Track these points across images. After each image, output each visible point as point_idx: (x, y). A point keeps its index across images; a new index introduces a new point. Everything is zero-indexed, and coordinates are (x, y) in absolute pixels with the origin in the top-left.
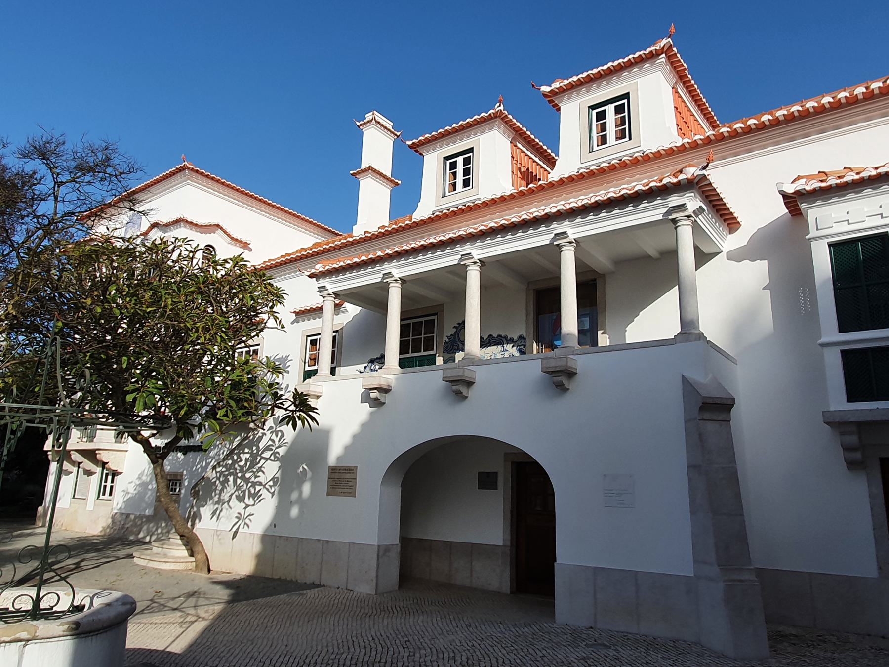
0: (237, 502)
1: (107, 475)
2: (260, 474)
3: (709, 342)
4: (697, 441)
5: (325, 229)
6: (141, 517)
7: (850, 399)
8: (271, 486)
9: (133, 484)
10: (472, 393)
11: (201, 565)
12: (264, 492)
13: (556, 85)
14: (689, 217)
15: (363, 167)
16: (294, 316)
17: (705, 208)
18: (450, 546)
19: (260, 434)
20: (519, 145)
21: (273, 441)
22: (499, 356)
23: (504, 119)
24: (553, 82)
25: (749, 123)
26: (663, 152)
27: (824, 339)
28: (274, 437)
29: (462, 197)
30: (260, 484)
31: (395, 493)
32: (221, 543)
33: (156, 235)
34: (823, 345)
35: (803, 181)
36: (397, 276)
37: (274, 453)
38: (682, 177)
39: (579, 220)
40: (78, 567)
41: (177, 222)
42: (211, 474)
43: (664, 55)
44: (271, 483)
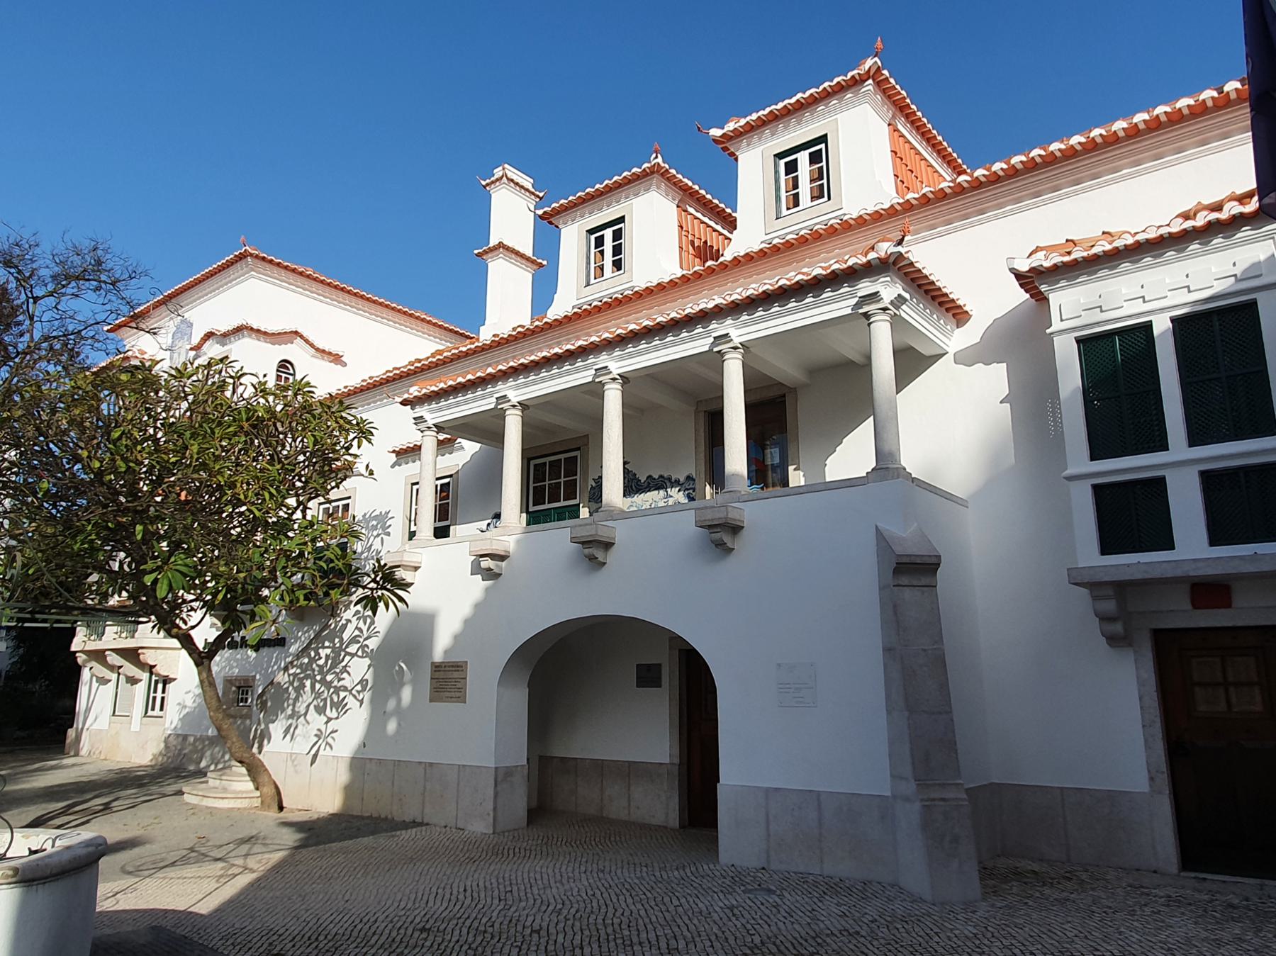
0: (316, 715)
1: (157, 682)
2: (345, 675)
3: (914, 479)
4: (893, 615)
5: (451, 331)
6: (202, 739)
7: (1214, 540)
8: (359, 692)
9: (191, 695)
10: (612, 557)
11: (268, 800)
12: (350, 700)
13: (730, 126)
14: (885, 309)
15: (491, 245)
16: (393, 457)
17: (907, 296)
18: (601, 768)
19: (344, 622)
20: (691, 210)
21: (361, 630)
22: (661, 504)
23: (664, 175)
24: (727, 122)
25: (1032, 155)
26: (867, 217)
27: (1070, 471)
28: (361, 625)
29: (612, 285)
30: (345, 689)
31: (519, 698)
32: (296, 772)
33: (213, 350)
34: (1070, 478)
35: (1041, 254)
36: (514, 400)
37: (363, 647)
38: (872, 255)
39: (744, 317)
40: (107, 807)
41: (239, 330)
42: (282, 678)
43: (870, 81)
44: (359, 688)
